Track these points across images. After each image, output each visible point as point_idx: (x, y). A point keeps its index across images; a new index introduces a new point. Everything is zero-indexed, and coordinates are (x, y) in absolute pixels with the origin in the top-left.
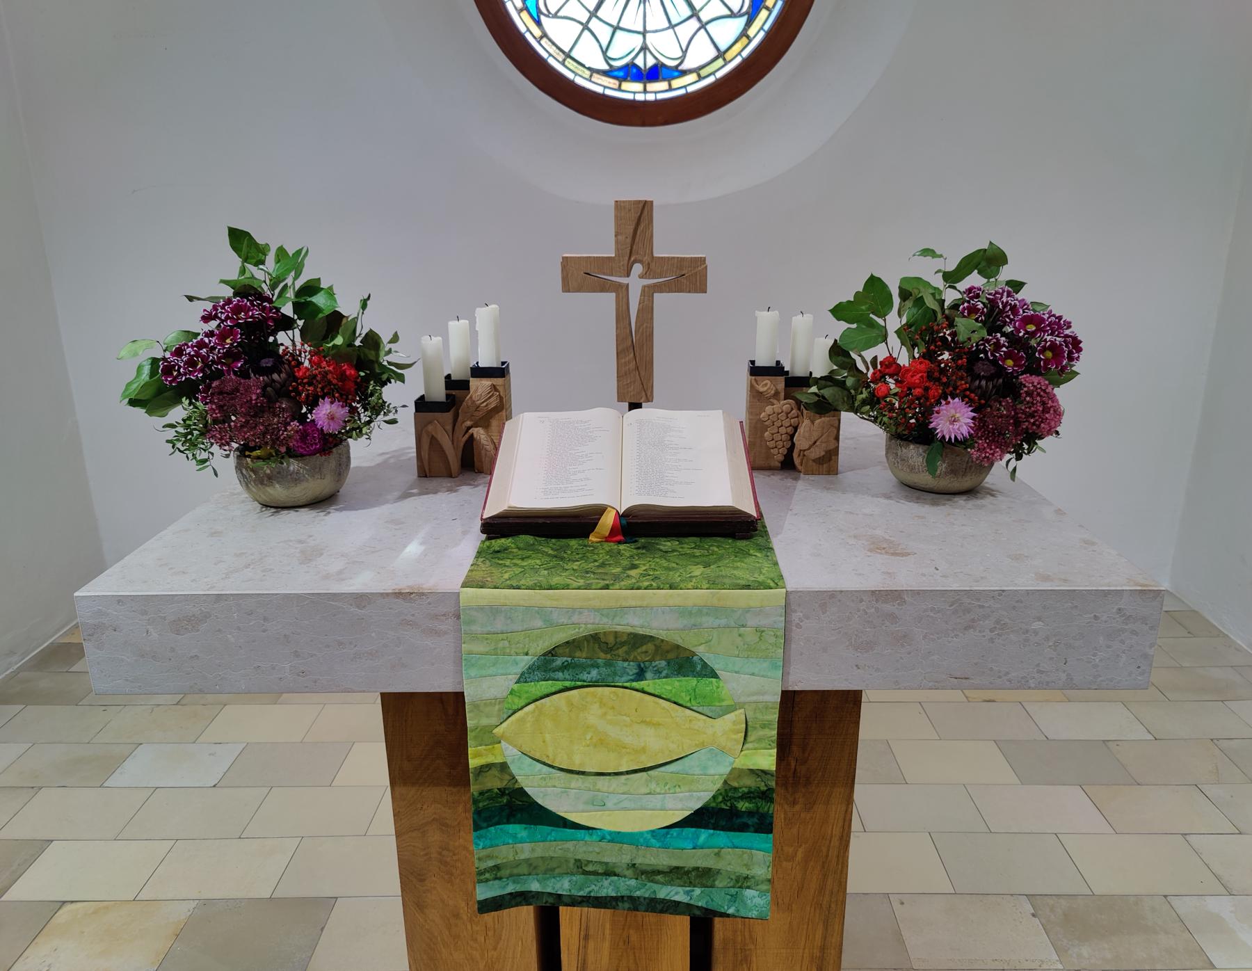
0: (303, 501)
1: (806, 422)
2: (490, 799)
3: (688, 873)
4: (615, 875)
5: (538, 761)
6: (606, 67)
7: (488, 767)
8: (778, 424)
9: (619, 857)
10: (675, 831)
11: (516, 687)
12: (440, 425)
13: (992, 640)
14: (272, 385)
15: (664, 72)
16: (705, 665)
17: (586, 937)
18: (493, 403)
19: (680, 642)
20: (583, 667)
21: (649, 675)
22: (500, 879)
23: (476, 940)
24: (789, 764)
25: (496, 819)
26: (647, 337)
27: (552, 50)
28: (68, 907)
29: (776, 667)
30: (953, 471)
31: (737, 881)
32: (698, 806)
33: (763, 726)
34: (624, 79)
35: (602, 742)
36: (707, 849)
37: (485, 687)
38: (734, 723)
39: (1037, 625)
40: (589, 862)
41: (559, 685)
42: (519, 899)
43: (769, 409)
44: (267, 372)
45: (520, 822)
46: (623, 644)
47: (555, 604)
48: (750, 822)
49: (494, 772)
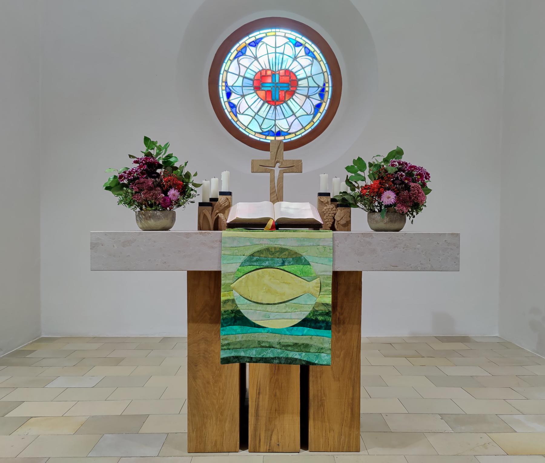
0: (159, 229)
1: (339, 211)
2: (228, 314)
3: (300, 346)
4: (273, 347)
5: (246, 299)
6: (261, 131)
7: (228, 300)
8: (329, 212)
9: (274, 339)
10: (295, 328)
11: (240, 268)
12: (207, 210)
13: (404, 252)
14: (153, 185)
15: (282, 133)
16: (306, 260)
17: (259, 393)
18: (227, 204)
19: (297, 251)
20: (264, 261)
21: (286, 264)
22: (230, 349)
23: (215, 394)
24: (336, 315)
25: (229, 323)
26: (281, 188)
27: (241, 125)
28: (32, 419)
29: (330, 261)
30: (391, 221)
31: (318, 350)
32: (304, 317)
33: (327, 286)
34: (268, 135)
35: (269, 291)
36: (308, 335)
37: (228, 268)
38: (316, 283)
39: (418, 246)
40: (263, 342)
41: (255, 268)
42: (236, 360)
43: (325, 208)
44: (155, 177)
45: (238, 325)
46: (278, 252)
47: (254, 237)
48: (323, 325)
49: (230, 303)
